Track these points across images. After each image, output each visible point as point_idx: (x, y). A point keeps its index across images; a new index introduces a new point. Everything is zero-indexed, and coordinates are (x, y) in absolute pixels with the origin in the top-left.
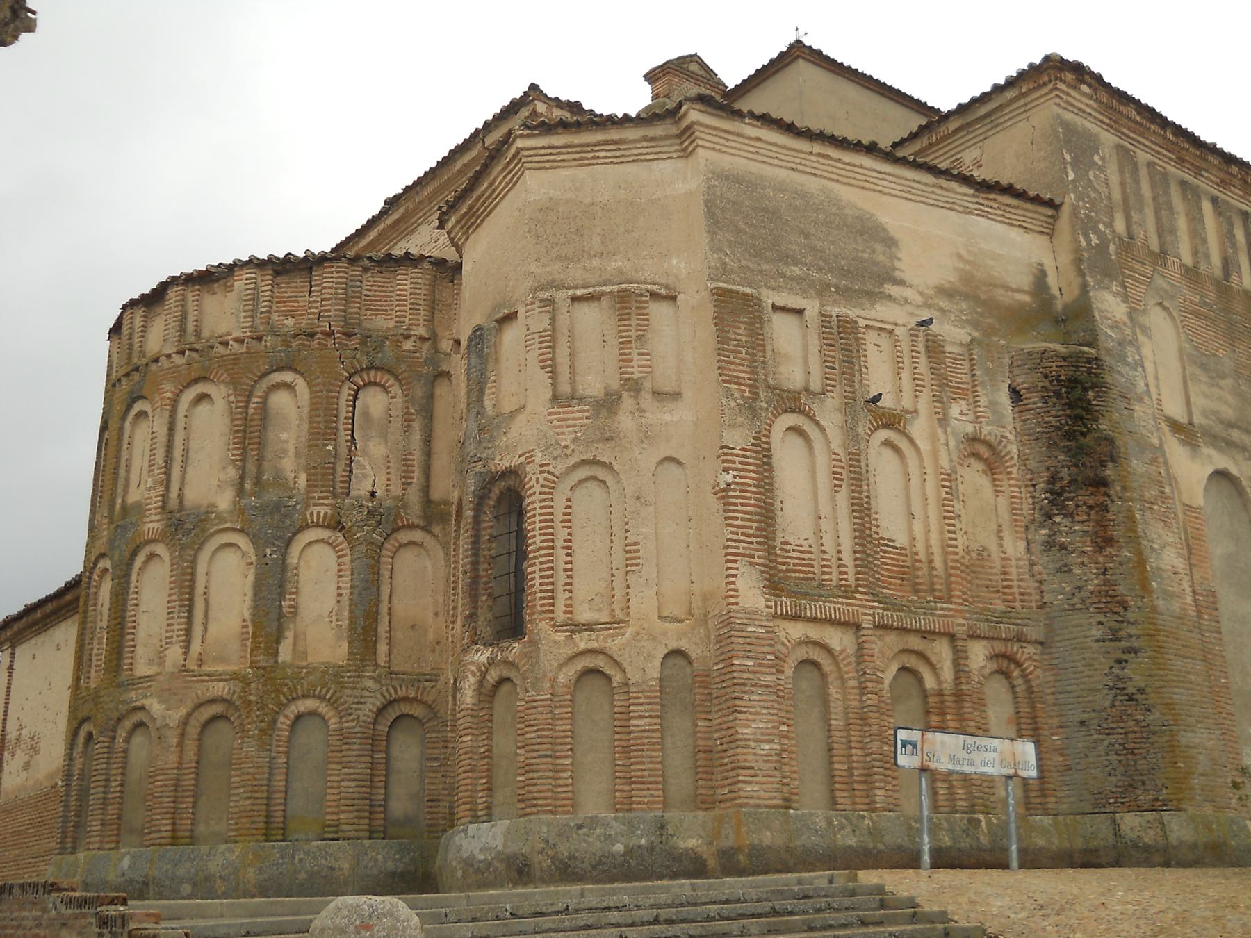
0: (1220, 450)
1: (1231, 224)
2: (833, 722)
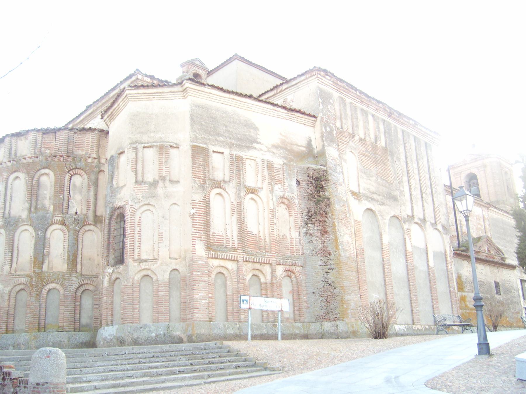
0: (369, 201)
1: (378, 123)
2: (228, 293)
